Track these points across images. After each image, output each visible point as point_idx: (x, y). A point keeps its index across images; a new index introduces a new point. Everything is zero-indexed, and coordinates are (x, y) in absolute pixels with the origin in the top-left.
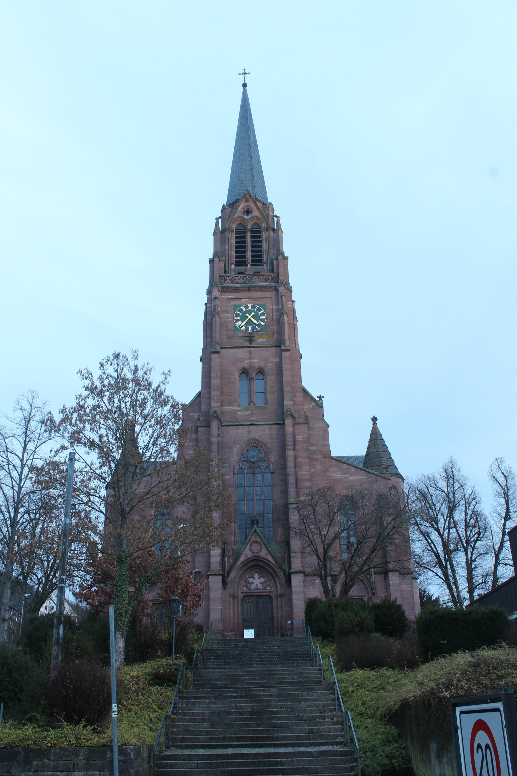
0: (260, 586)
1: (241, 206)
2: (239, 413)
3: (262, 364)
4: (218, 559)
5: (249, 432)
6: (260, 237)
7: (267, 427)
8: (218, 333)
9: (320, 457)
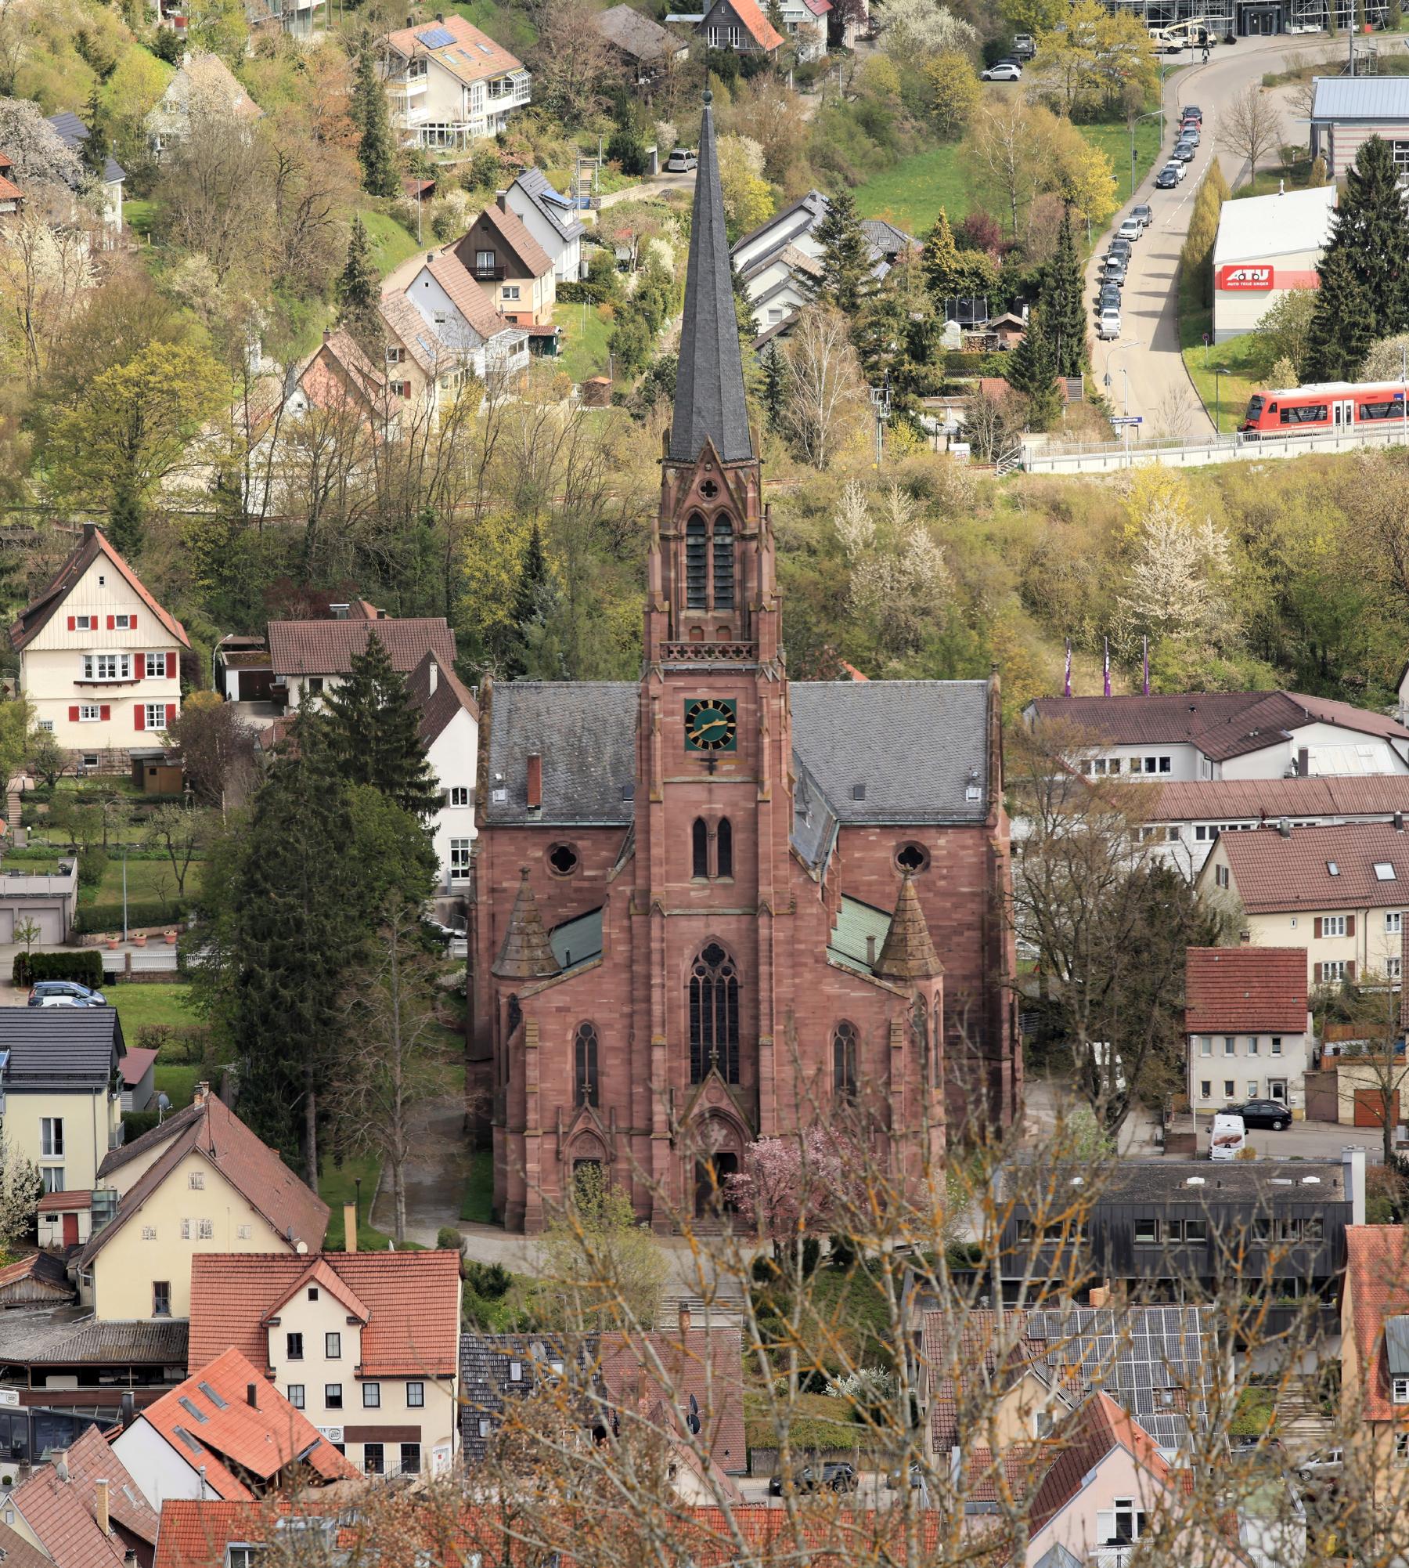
1: (697, 480)
3: (728, 814)
5: (707, 926)
6: (700, 825)
9: (810, 961)
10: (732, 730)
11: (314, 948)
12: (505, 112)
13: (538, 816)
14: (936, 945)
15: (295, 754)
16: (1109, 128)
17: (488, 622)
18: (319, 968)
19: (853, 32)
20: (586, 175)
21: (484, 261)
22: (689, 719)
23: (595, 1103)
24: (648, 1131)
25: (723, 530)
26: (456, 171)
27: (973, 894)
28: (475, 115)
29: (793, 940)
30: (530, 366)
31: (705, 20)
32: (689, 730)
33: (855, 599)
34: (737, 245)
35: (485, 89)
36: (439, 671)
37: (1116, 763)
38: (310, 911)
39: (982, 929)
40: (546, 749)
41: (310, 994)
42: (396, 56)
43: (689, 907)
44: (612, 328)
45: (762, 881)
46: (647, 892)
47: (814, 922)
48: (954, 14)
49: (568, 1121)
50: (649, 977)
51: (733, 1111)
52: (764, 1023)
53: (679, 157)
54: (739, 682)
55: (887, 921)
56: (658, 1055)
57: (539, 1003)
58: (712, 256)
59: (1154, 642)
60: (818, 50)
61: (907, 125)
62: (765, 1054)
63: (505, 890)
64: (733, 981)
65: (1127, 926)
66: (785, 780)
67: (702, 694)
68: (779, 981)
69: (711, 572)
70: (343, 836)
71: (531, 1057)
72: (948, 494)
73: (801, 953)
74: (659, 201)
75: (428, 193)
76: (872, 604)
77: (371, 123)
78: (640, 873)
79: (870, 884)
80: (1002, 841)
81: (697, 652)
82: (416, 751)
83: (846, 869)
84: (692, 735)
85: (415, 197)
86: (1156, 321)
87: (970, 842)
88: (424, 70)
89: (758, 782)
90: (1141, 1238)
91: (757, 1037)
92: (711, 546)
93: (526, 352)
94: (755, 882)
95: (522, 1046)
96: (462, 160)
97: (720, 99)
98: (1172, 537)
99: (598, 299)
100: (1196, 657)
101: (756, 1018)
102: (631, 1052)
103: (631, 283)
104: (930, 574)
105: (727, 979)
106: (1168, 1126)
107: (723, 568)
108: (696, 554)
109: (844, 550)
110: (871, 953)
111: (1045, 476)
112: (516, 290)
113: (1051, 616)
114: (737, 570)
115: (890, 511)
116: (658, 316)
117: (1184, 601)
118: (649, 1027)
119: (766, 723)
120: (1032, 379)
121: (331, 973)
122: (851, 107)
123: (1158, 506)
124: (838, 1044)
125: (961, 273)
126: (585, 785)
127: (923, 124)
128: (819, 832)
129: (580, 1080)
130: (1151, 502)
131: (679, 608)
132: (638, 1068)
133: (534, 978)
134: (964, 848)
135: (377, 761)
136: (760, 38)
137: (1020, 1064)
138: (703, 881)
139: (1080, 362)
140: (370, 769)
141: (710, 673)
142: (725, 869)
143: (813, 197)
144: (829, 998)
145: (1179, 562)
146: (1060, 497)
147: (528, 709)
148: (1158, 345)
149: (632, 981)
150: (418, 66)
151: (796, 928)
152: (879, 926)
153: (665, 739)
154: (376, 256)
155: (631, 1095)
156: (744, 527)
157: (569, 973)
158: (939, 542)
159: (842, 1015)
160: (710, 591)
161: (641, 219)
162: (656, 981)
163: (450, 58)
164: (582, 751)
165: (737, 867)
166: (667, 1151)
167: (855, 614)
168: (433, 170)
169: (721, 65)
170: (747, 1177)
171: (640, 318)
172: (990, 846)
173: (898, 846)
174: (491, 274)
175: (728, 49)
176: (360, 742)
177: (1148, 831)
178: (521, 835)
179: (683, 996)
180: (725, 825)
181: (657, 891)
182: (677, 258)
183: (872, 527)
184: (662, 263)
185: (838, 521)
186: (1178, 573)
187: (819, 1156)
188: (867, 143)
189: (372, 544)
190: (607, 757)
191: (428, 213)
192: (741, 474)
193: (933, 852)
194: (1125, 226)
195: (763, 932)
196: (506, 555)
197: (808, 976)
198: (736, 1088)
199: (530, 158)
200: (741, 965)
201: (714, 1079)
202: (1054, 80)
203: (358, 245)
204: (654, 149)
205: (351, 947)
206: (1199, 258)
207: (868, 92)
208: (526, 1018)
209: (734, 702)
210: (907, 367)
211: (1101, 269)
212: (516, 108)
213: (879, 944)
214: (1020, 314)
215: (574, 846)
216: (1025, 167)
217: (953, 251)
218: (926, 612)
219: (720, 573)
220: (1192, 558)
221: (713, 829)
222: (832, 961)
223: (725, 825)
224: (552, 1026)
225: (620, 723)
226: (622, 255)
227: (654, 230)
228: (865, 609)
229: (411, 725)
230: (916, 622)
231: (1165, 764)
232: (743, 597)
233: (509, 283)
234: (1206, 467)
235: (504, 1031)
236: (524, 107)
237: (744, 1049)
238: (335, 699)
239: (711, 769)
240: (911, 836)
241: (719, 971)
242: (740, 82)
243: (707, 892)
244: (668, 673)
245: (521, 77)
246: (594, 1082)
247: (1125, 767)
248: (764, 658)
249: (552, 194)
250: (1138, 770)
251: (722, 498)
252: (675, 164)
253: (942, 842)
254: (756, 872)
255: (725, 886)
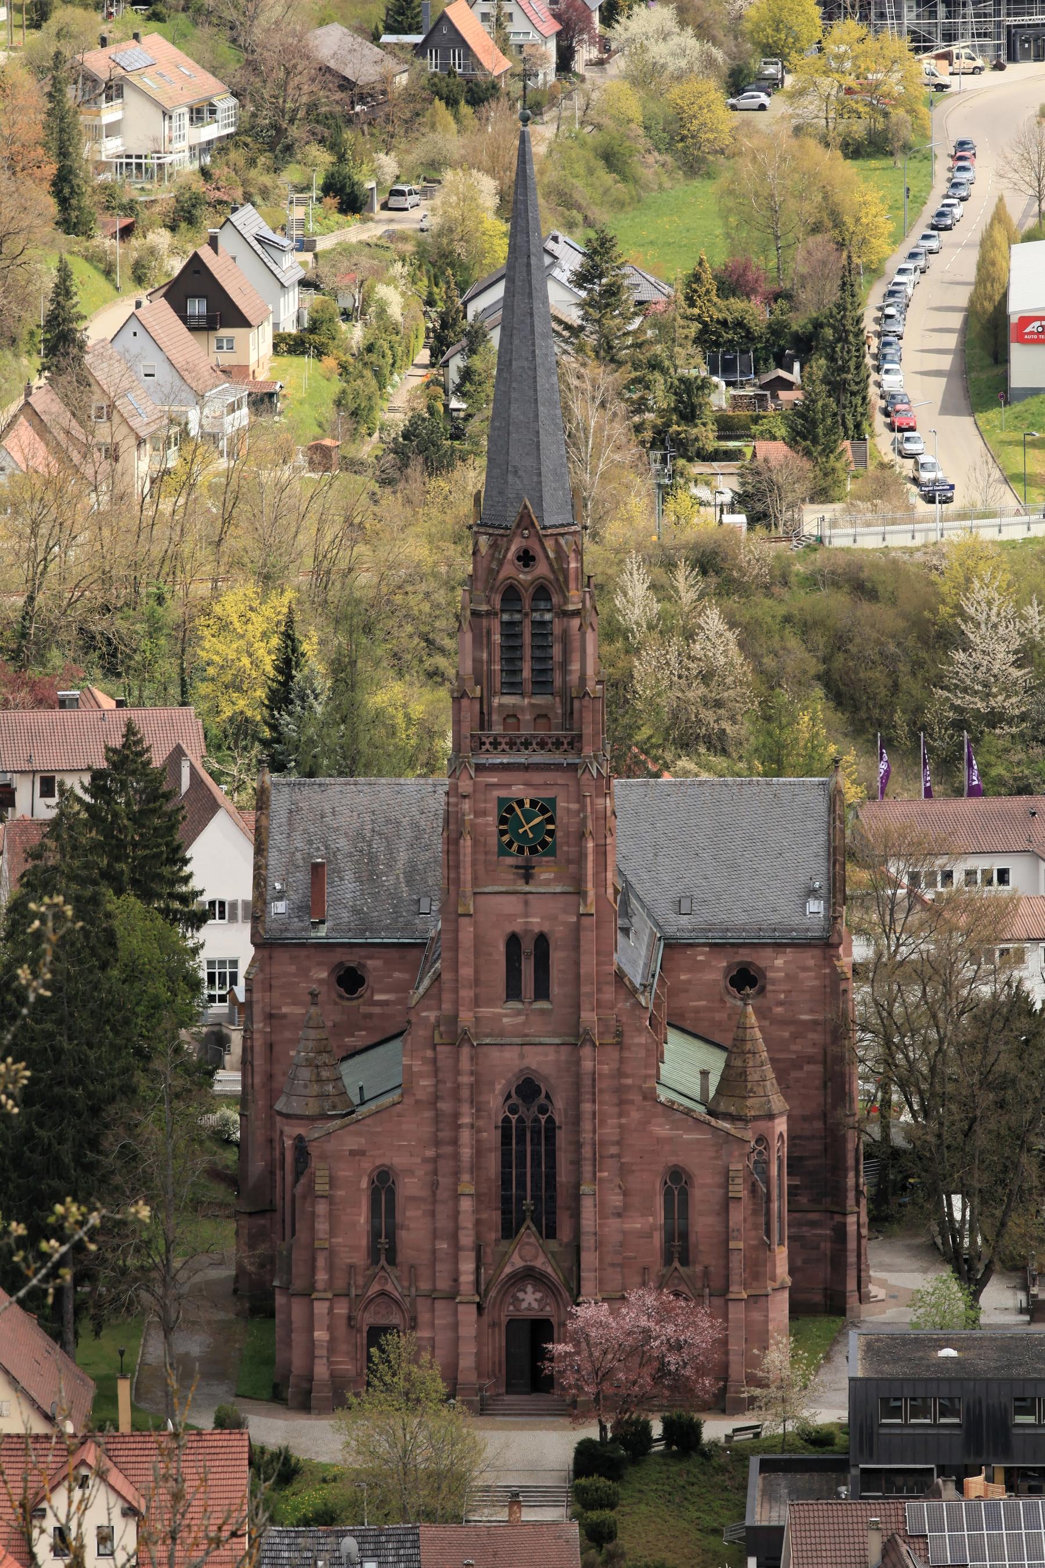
0: (535, 1305)
1: (513, 548)
2: (505, 1020)
3: (546, 928)
4: (471, 1278)
5: (522, 1056)
6: (513, 942)
7: (552, 1048)
8: (469, 870)
9: (637, 1098)
10: (551, 833)
11: (75, 1083)
12: (209, 143)
13: (323, 931)
14: (779, 1080)
15: (53, 859)
16: (873, 163)
17: (228, 712)
18: (80, 1106)
19: (585, 54)
20: (298, 212)
21: (197, 307)
22: (503, 821)
23: (392, 1261)
24: (452, 1296)
25: (542, 605)
26: (157, 209)
27: (815, 1022)
28: (179, 145)
29: (620, 1074)
30: (252, 427)
31: (425, 41)
32: (502, 833)
33: (639, 688)
34: (469, 293)
35: (187, 117)
36: (192, 767)
37: (948, 876)
38: (70, 1039)
39: (825, 1063)
40: (332, 854)
41: (71, 1132)
42: (91, 79)
43: (501, 1035)
44: (337, 386)
45: (585, 1005)
46: (454, 1018)
47: (642, 1054)
48: (698, 37)
49: (360, 1281)
50: (456, 1115)
51: (549, 1270)
52: (587, 1168)
53: (401, 193)
54: (560, 778)
55: (725, 1055)
56: (466, 1205)
57: (331, 1146)
58: (530, 294)
59: (976, 740)
60: (547, 73)
61: (650, 159)
62: (588, 1207)
63: (284, 1016)
64: (550, 1120)
65: (990, 1059)
66: (610, 890)
67: (518, 791)
68: (602, 1122)
69: (527, 652)
70: (105, 954)
71: (322, 1208)
72: (740, 569)
73: (629, 1088)
74: (383, 242)
75: (126, 232)
76: (659, 695)
77: (63, 153)
78: (447, 996)
79: (697, 1010)
80: (845, 963)
81: (511, 744)
82: (177, 857)
83: (672, 993)
84: (506, 838)
85: (113, 236)
86: (943, 381)
87: (811, 963)
88: (120, 95)
89: (580, 893)
90: (1020, 1419)
91: (577, 1185)
92: (527, 623)
93: (245, 410)
94: (577, 1007)
95: (310, 1192)
96: (164, 194)
97: (446, 129)
98: (994, 619)
99: (320, 353)
100: (1022, 756)
101: (577, 1163)
102: (434, 1202)
103: (355, 334)
104: (722, 660)
105: (543, 1118)
106: (1034, 1290)
107: (542, 650)
108: (511, 631)
109: (624, 633)
110: (705, 1089)
111: (847, 550)
112: (230, 341)
113: (856, 709)
114: (557, 651)
115: (676, 590)
116: (386, 372)
117: (1008, 690)
118: (456, 1174)
119: (590, 826)
120: (815, 441)
121: (95, 1111)
122: (589, 140)
123: (977, 584)
124: (668, 1194)
125: (724, 323)
126: (375, 896)
127: (668, 158)
128: (643, 952)
129: (375, 1234)
130: (968, 580)
131: (492, 694)
132: (443, 1222)
133: (324, 1117)
134: (805, 969)
135: (133, 870)
136: (487, 64)
137: (864, 1219)
138: (519, 1005)
139: (865, 425)
140: (125, 878)
141: (527, 768)
142: (542, 991)
143: (555, 239)
144: (660, 1141)
145: (1002, 648)
146: (864, 575)
147: (311, 810)
148: (946, 409)
149: (437, 1120)
150: (114, 90)
151: (622, 1061)
152: (715, 1062)
153: (475, 842)
154: (81, 301)
155: (434, 1252)
156: (566, 600)
157: (364, 1110)
158: (732, 625)
159: (673, 1160)
160: (526, 674)
161: (365, 262)
162: (466, 1120)
163: (148, 83)
164: (372, 858)
165: (555, 990)
166: (474, 1316)
167: (640, 706)
168: (130, 208)
169: (445, 91)
170: (569, 1348)
171: (368, 373)
172: (834, 968)
173: (729, 968)
174: (203, 323)
175: (451, 73)
176: (116, 849)
177: (1004, 952)
178: (303, 953)
179: (492, 1137)
180: (542, 941)
181: (466, 1017)
182: (406, 306)
183: (657, 607)
184: (390, 311)
185: (619, 601)
186: (1001, 658)
187: (652, 1324)
188: (608, 179)
189: (98, 625)
190: (400, 865)
191: (125, 255)
192: (562, 541)
193: (770, 975)
194: (902, 271)
195: (587, 1065)
196: (249, 635)
197: (635, 1115)
198: (553, 1245)
199: (238, 193)
200: (559, 1104)
201: (528, 1235)
202: (811, 108)
203: (63, 290)
204: (373, 184)
205: (116, 1081)
206: (989, 307)
207: (606, 121)
208: (314, 1163)
209: (553, 801)
210: (675, 427)
211: (877, 320)
212: (220, 139)
213: (714, 1081)
214: (790, 370)
215: (364, 966)
216: (792, 204)
217: (715, 299)
218: (718, 704)
219: (538, 653)
220: (1017, 643)
221: (528, 946)
222: (662, 1099)
223: (542, 941)
224: (344, 1173)
225: (415, 826)
226: (346, 303)
227: (379, 274)
228: (650, 701)
229: (171, 828)
230: (708, 715)
231: (1003, 876)
232: (564, 682)
233: (224, 332)
234: (1027, 541)
235: (289, 1178)
236: (229, 136)
237: (562, 1198)
238: (87, 798)
239: (528, 878)
240: (744, 956)
241: (534, 1109)
242: (465, 109)
243: (521, 1019)
244: (480, 768)
245: (226, 104)
246: (391, 1236)
247: (958, 877)
248: (588, 751)
249: (267, 233)
250: (990, 883)
251: (541, 569)
252: (394, 202)
253: (779, 962)
254: (578, 996)
255: (543, 1012)
